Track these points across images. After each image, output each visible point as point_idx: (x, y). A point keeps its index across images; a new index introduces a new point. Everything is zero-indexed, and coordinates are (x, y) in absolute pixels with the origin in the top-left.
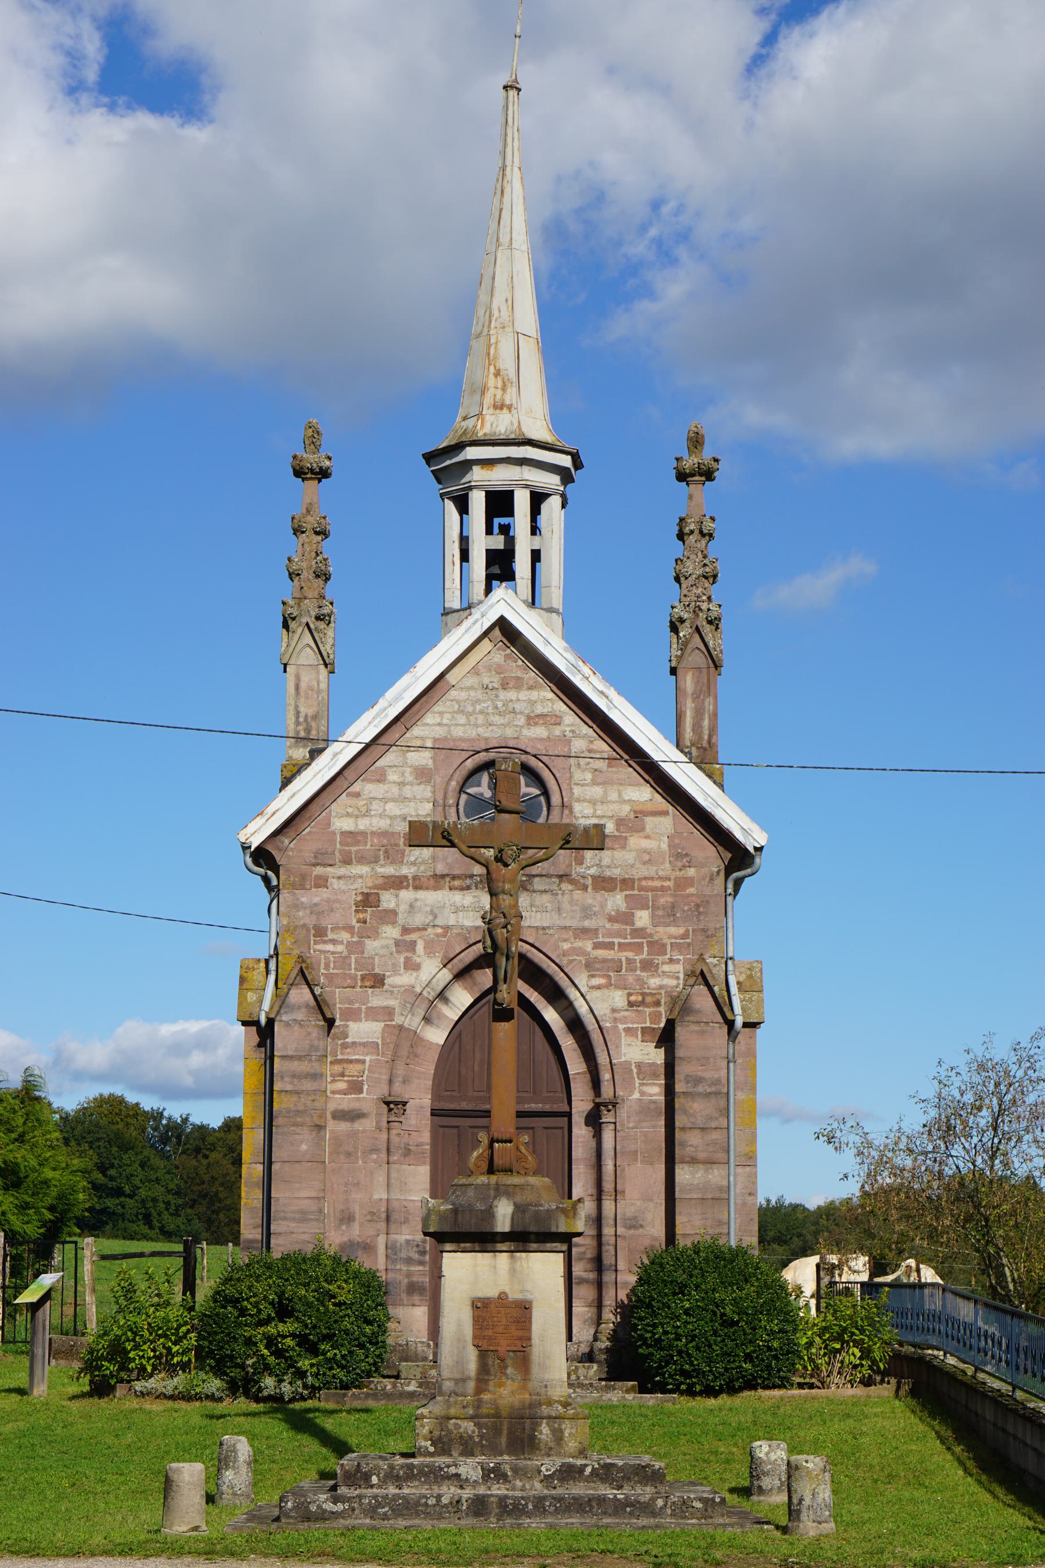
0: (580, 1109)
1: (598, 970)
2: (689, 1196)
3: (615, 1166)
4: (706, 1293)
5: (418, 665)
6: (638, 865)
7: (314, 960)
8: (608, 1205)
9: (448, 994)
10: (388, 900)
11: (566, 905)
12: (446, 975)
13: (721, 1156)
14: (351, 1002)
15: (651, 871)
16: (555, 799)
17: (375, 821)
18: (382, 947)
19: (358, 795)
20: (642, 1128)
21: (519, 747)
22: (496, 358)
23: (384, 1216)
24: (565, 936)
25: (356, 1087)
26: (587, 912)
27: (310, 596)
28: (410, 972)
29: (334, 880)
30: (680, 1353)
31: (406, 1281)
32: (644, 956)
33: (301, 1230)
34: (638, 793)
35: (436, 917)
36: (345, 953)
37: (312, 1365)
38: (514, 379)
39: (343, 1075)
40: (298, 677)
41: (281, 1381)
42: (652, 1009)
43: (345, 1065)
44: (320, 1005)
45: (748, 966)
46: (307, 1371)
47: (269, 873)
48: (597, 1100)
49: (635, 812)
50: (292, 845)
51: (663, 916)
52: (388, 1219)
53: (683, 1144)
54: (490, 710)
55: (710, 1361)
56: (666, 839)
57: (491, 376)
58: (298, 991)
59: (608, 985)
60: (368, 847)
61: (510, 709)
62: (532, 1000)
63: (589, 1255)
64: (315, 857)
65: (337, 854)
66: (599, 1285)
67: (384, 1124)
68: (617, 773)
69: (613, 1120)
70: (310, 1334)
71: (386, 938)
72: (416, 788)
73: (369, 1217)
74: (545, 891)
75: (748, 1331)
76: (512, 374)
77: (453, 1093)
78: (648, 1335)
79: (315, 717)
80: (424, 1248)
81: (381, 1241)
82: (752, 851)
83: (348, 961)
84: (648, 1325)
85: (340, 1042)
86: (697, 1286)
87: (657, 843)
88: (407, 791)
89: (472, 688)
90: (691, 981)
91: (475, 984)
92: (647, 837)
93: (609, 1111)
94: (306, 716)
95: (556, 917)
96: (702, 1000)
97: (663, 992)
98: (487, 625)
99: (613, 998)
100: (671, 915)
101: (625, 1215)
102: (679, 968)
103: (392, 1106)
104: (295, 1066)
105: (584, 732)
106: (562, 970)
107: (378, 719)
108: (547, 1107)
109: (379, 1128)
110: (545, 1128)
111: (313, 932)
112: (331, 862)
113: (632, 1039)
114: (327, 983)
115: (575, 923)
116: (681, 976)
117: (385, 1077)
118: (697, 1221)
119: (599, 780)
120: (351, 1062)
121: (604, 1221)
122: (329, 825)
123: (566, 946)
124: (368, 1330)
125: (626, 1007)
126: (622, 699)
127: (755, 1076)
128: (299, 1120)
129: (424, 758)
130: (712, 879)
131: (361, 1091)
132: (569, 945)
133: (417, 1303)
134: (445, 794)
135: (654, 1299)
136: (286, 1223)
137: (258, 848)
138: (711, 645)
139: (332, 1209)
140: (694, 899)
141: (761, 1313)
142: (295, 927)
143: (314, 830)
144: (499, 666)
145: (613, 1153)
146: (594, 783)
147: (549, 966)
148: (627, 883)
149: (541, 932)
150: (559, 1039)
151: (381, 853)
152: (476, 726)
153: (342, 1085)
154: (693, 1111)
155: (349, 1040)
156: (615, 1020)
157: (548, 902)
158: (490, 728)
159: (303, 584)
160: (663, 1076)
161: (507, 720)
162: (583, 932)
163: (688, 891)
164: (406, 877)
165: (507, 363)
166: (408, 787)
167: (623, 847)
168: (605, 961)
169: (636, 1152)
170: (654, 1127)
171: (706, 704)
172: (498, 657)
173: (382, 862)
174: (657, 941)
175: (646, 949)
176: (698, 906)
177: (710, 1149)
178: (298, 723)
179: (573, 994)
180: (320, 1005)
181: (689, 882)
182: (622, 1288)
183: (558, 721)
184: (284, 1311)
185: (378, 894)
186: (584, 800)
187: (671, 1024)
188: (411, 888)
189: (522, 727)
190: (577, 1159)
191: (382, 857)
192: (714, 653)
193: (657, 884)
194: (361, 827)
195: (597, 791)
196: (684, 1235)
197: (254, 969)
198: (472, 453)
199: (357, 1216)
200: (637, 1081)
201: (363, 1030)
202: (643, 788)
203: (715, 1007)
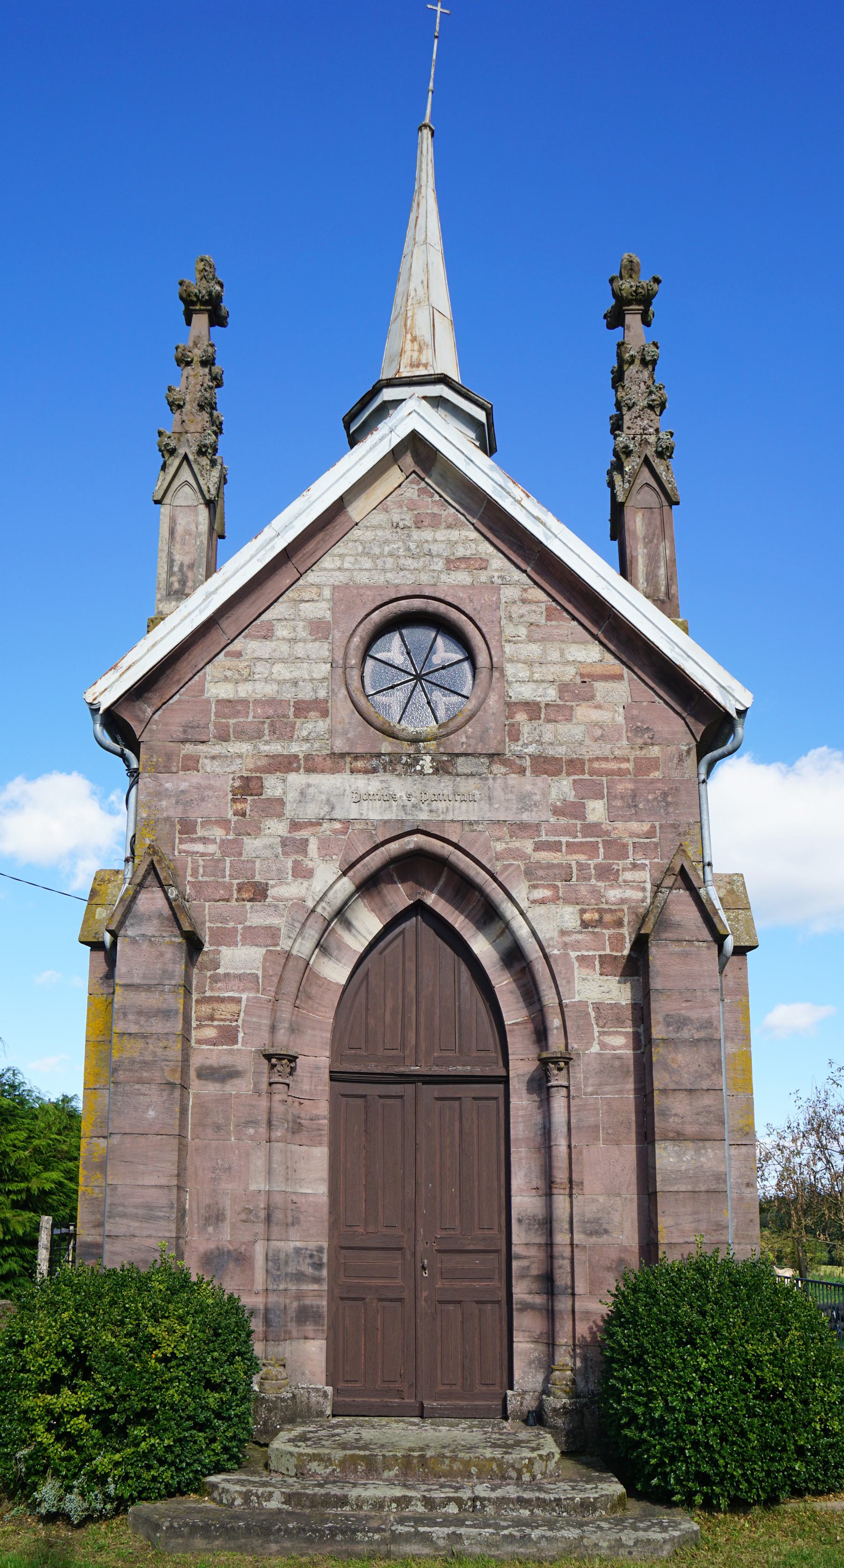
0: (520, 1072)
1: (542, 878)
2: (675, 1188)
3: (569, 1147)
4: (732, 1343)
5: (313, 487)
6: (588, 742)
7: (178, 864)
8: (561, 1202)
9: (349, 914)
10: (273, 786)
11: (498, 793)
12: (346, 886)
13: (714, 1129)
14: (225, 920)
15: (605, 750)
16: (482, 659)
17: (259, 686)
18: (265, 847)
19: (239, 655)
20: (604, 1093)
21: (437, 595)
22: (412, 328)
23: (262, 1214)
24: (498, 833)
25: (228, 1035)
26: (525, 801)
27: (192, 430)
28: (300, 880)
29: (207, 761)
30: (696, 1445)
31: (295, 1304)
32: (600, 860)
33: (145, 1233)
34: (584, 652)
35: (333, 808)
36: (218, 855)
37: (117, 1464)
38: (430, 342)
39: (212, 1018)
40: (173, 520)
41: (69, 1489)
42: (612, 931)
43: (215, 1005)
44: (176, 913)
45: (727, 880)
46: (107, 1475)
47: (127, 751)
48: (545, 1055)
49: (582, 675)
50: (156, 717)
51: (622, 808)
52: (268, 1219)
53: (664, 1114)
54: (401, 552)
55: (743, 1459)
56: (621, 710)
57: (408, 343)
58: (149, 895)
59: (555, 899)
60: (250, 719)
61: (426, 551)
62: (456, 926)
63: (534, 1272)
64: (185, 732)
65: (211, 727)
66: (551, 1315)
67: (264, 1086)
68: (557, 627)
69: (565, 1083)
70: (112, 1411)
71: (270, 835)
72: (310, 645)
73: (243, 1216)
74: (472, 775)
75: (799, 1406)
76: (428, 338)
77: (358, 1051)
78: (639, 1410)
79: (191, 566)
80: (321, 1259)
81: (259, 1250)
82: (734, 715)
83: (221, 866)
84: (639, 1393)
85: (209, 974)
86: (715, 1333)
87: (610, 715)
88: (300, 650)
89: (380, 527)
90: (669, 881)
91: (385, 905)
92: (598, 707)
93: (560, 1069)
94: (182, 565)
95: (486, 807)
96: (683, 910)
97: (625, 907)
98: (396, 440)
99: (562, 916)
100: (631, 806)
101: (583, 1216)
102: (645, 876)
103: (274, 1061)
104: (143, 999)
105: (516, 578)
106: (495, 879)
107: (263, 552)
108: (478, 1071)
109: (257, 1092)
110: (474, 1098)
111: (178, 827)
112: (204, 738)
113: (587, 971)
114: (194, 895)
115: (510, 817)
116: (648, 886)
117: (266, 1022)
118: (687, 1224)
119: (536, 636)
120: (222, 1000)
121: (555, 1225)
122: (202, 691)
123: (499, 847)
124: (213, 1399)
125: (579, 928)
126: (562, 527)
127: (748, 1022)
128: (145, 1074)
129: (320, 610)
130: (681, 760)
131: (235, 1042)
132: (504, 846)
133: (311, 1335)
134: (346, 654)
135: (646, 1352)
136: (125, 1221)
137: (108, 710)
138: (664, 477)
139: (195, 1203)
140: (659, 785)
141: (815, 1376)
142: (157, 821)
143: (184, 698)
144: (411, 500)
145: (565, 1129)
146: (530, 640)
147: (478, 873)
148: (574, 765)
149: (467, 828)
150: (491, 977)
151: (266, 726)
152: (384, 570)
153: (210, 1033)
154: (675, 1065)
155: (221, 971)
156: (565, 945)
157: (476, 788)
158: (402, 573)
159: (185, 418)
160: (629, 1023)
161: (421, 563)
162: (521, 828)
163: (651, 776)
164: (296, 757)
165: (423, 330)
166: (301, 644)
167: (569, 720)
168: (550, 866)
169: (597, 1127)
170: (620, 1092)
171: (661, 549)
172: (411, 491)
173: (266, 738)
174: (615, 841)
175: (601, 850)
176: (665, 795)
177: (702, 1120)
178: (170, 573)
179: (509, 910)
180: (176, 913)
181: (654, 764)
182: (582, 1320)
183: (483, 565)
184: (79, 1364)
185: (260, 778)
186: (519, 661)
187: (641, 944)
188: (302, 770)
189: (441, 572)
190: (517, 1139)
191: (266, 732)
192: (668, 487)
193: (613, 766)
194: (242, 694)
195: (534, 649)
196: (670, 1245)
197: (109, 881)
198: (388, 394)
199: (228, 1213)
200: (596, 1029)
201: (239, 958)
202: (590, 647)
203: (700, 920)
